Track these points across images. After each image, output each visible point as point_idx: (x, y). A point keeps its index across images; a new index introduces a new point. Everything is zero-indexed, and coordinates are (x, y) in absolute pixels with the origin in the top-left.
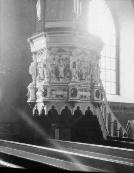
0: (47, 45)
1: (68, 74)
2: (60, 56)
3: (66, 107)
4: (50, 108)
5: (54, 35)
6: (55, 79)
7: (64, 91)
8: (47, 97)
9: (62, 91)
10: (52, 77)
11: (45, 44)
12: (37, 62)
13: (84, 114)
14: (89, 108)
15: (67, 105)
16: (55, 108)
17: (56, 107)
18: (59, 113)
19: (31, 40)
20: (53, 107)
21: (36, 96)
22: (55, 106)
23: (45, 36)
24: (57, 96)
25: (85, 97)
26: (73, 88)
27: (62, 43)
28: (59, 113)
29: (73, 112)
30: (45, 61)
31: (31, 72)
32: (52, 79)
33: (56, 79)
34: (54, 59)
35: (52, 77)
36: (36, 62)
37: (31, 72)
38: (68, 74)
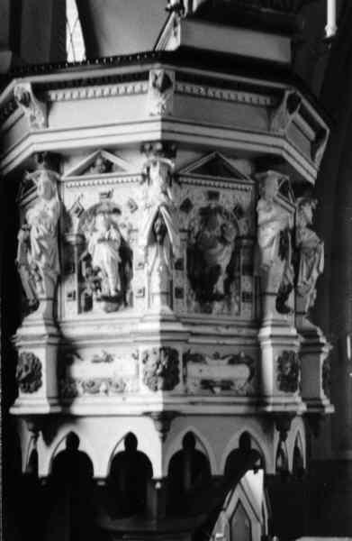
0: (163, 131)
1: (246, 285)
2: (213, 196)
3: (245, 438)
4: (177, 445)
5: (196, 89)
6: (189, 303)
7: (235, 360)
8: (179, 388)
9: (226, 361)
10: (179, 293)
11: (158, 126)
12: (63, 208)
13: (101, 469)
14: (131, 440)
15: (251, 431)
16: (198, 447)
17: (203, 439)
18: (218, 468)
19: (41, 92)
20: (190, 439)
21: (72, 381)
22: (197, 432)
23: (165, 86)
24: (207, 385)
25: (227, 385)
26: (289, 349)
27: (221, 133)
28: (101, 469)
29: (218, 464)
30: (163, 210)
31: (39, 257)
32: (180, 300)
33: (194, 304)
34: (186, 206)
35: (179, 293)
36: (59, 210)
37: (39, 257)
38: (246, 285)
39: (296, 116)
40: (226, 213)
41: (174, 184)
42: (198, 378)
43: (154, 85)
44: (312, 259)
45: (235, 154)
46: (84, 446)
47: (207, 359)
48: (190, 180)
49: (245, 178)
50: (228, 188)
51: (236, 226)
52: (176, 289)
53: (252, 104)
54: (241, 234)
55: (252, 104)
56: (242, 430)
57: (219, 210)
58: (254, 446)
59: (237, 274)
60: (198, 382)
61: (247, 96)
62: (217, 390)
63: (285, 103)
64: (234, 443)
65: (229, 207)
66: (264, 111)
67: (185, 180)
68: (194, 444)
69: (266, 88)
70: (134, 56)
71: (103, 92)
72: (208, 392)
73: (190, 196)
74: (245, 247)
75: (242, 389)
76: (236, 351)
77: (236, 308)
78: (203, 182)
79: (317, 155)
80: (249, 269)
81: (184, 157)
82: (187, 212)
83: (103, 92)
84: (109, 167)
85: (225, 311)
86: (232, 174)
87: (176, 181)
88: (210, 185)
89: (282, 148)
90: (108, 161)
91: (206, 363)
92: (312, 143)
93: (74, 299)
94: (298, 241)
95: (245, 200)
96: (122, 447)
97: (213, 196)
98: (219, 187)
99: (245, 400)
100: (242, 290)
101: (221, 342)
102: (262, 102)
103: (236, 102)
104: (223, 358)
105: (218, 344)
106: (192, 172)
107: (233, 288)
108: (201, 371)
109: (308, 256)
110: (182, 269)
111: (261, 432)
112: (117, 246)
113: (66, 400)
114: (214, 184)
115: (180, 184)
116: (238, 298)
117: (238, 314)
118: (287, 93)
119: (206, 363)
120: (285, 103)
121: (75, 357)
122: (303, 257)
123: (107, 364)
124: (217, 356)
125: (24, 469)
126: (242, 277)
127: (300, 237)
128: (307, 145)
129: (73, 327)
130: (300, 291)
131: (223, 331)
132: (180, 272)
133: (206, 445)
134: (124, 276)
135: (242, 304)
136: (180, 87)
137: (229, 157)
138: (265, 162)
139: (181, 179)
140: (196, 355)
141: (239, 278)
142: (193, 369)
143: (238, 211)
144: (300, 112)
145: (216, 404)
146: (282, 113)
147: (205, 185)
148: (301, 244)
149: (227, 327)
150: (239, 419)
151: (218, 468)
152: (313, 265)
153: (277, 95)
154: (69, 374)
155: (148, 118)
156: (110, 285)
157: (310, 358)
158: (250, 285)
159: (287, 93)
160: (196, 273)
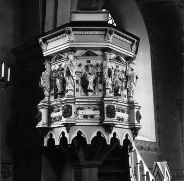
3: (99, 133)
5: (80, 33)
9: (92, 109)
15: (100, 131)
18: (89, 142)
24: (85, 117)
25: (92, 117)
33: (83, 93)
39: (114, 35)
40: (94, 66)
41: (76, 60)
42: (82, 115)
43: (67, 33)
44: (131, 79)
45: (96, 49)
46: (54, 137)
47: (85, 109)
48: (80, 58)
49: (99, 56)
50: (93, 59)
51: (97, 69)
52: (76, 89)
53: (99, 34)
54: (98, 72)
55: (99, 34)
56: (98, 130)
57: (91, 66)
58: (102, 136)
59: (97, 83)
60: (82, 116)
61: (97, 33)
62: (89, 118)
63: (108, 32)
64: (95, 134)
65: (94, 64)
66: (103, 36)
67: (79, 58)
68: (81, 134)
69: (126, 34)
70: (60, 27)
71: (54, 39)
72: (86, 119)
73: (81, 62)
74: (100, 76)
75: (98, 118)
76: (95, 106)
77: (97, 94)
78: (85, 58)
79: (133, 48)
80: (101, 82)
81: (78, 53)
82: (80, 67)
83: (54, 39)
84: (61, 57)
85: (94, 95)
86: (95, 55)
87: (77, 58)
88: (87, 59)
89: (109, 45)
90: (60, 56)
91: (85, 110)
92: (131, 45)
93: (53, 95)
94: (127, 74)
95: (99, 62)
96: (61, 136)
97: (88, 62)
98: (90, 59)
99: (99, 121)
100: (99, 88)
101: (90, 104)
102: (102, 33)
103: (93, 34)
104: (91, 109)
105: (89, 104)
106: (82, 55)
107: (96, 88)
108: (83, 112)
109: (130, 79)
110: (79, 83)
111: (104, 131)
112: (62, 79)
113: (50, 124)
114: (88, 58)
115: (78, 59)
116: (98, 91)
117: (98, 95)
118: (108, 30)
119: (85, 110)
120: (108, 32)
121: (52, 111)
122: (129, 79)
123: (58, 113)
124: (89, 108)
125: (45, 145)
126: (99, 84)
127: (127, 73)
128: (130, 46)
129: (52, 103)
130: (129, 90)
131: (91, 100)
132: (78, 84)
133: (84, 134)
134: (64, 87)
135: (99, 93)
136: (75, 32)
137: (94, 50)
138: (105, 50)
139: (78, 58)
140: (82, 108)
141: (98, 85)
142: (80, 112)
143: (97, 65)
144: (115, 33)
145: (88, 122)
146: (108, 35)
147: (86, 59)
148: (128, 75)
149: (92, 99)
150: (96, 127)
151: (89, 142)
152: (132, 81)
153: (106, 30)
154: (51, 116)
155: (66, 42)
156: (60, 90)
157: (132, 110)
158: (101, 87)
159: (108, 30)
160: (84, 84)
